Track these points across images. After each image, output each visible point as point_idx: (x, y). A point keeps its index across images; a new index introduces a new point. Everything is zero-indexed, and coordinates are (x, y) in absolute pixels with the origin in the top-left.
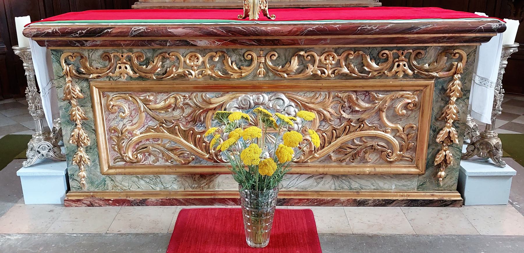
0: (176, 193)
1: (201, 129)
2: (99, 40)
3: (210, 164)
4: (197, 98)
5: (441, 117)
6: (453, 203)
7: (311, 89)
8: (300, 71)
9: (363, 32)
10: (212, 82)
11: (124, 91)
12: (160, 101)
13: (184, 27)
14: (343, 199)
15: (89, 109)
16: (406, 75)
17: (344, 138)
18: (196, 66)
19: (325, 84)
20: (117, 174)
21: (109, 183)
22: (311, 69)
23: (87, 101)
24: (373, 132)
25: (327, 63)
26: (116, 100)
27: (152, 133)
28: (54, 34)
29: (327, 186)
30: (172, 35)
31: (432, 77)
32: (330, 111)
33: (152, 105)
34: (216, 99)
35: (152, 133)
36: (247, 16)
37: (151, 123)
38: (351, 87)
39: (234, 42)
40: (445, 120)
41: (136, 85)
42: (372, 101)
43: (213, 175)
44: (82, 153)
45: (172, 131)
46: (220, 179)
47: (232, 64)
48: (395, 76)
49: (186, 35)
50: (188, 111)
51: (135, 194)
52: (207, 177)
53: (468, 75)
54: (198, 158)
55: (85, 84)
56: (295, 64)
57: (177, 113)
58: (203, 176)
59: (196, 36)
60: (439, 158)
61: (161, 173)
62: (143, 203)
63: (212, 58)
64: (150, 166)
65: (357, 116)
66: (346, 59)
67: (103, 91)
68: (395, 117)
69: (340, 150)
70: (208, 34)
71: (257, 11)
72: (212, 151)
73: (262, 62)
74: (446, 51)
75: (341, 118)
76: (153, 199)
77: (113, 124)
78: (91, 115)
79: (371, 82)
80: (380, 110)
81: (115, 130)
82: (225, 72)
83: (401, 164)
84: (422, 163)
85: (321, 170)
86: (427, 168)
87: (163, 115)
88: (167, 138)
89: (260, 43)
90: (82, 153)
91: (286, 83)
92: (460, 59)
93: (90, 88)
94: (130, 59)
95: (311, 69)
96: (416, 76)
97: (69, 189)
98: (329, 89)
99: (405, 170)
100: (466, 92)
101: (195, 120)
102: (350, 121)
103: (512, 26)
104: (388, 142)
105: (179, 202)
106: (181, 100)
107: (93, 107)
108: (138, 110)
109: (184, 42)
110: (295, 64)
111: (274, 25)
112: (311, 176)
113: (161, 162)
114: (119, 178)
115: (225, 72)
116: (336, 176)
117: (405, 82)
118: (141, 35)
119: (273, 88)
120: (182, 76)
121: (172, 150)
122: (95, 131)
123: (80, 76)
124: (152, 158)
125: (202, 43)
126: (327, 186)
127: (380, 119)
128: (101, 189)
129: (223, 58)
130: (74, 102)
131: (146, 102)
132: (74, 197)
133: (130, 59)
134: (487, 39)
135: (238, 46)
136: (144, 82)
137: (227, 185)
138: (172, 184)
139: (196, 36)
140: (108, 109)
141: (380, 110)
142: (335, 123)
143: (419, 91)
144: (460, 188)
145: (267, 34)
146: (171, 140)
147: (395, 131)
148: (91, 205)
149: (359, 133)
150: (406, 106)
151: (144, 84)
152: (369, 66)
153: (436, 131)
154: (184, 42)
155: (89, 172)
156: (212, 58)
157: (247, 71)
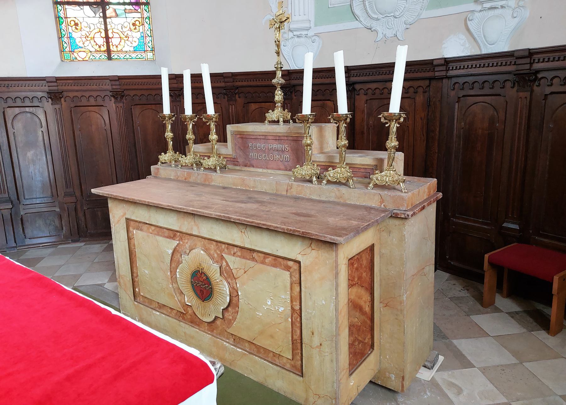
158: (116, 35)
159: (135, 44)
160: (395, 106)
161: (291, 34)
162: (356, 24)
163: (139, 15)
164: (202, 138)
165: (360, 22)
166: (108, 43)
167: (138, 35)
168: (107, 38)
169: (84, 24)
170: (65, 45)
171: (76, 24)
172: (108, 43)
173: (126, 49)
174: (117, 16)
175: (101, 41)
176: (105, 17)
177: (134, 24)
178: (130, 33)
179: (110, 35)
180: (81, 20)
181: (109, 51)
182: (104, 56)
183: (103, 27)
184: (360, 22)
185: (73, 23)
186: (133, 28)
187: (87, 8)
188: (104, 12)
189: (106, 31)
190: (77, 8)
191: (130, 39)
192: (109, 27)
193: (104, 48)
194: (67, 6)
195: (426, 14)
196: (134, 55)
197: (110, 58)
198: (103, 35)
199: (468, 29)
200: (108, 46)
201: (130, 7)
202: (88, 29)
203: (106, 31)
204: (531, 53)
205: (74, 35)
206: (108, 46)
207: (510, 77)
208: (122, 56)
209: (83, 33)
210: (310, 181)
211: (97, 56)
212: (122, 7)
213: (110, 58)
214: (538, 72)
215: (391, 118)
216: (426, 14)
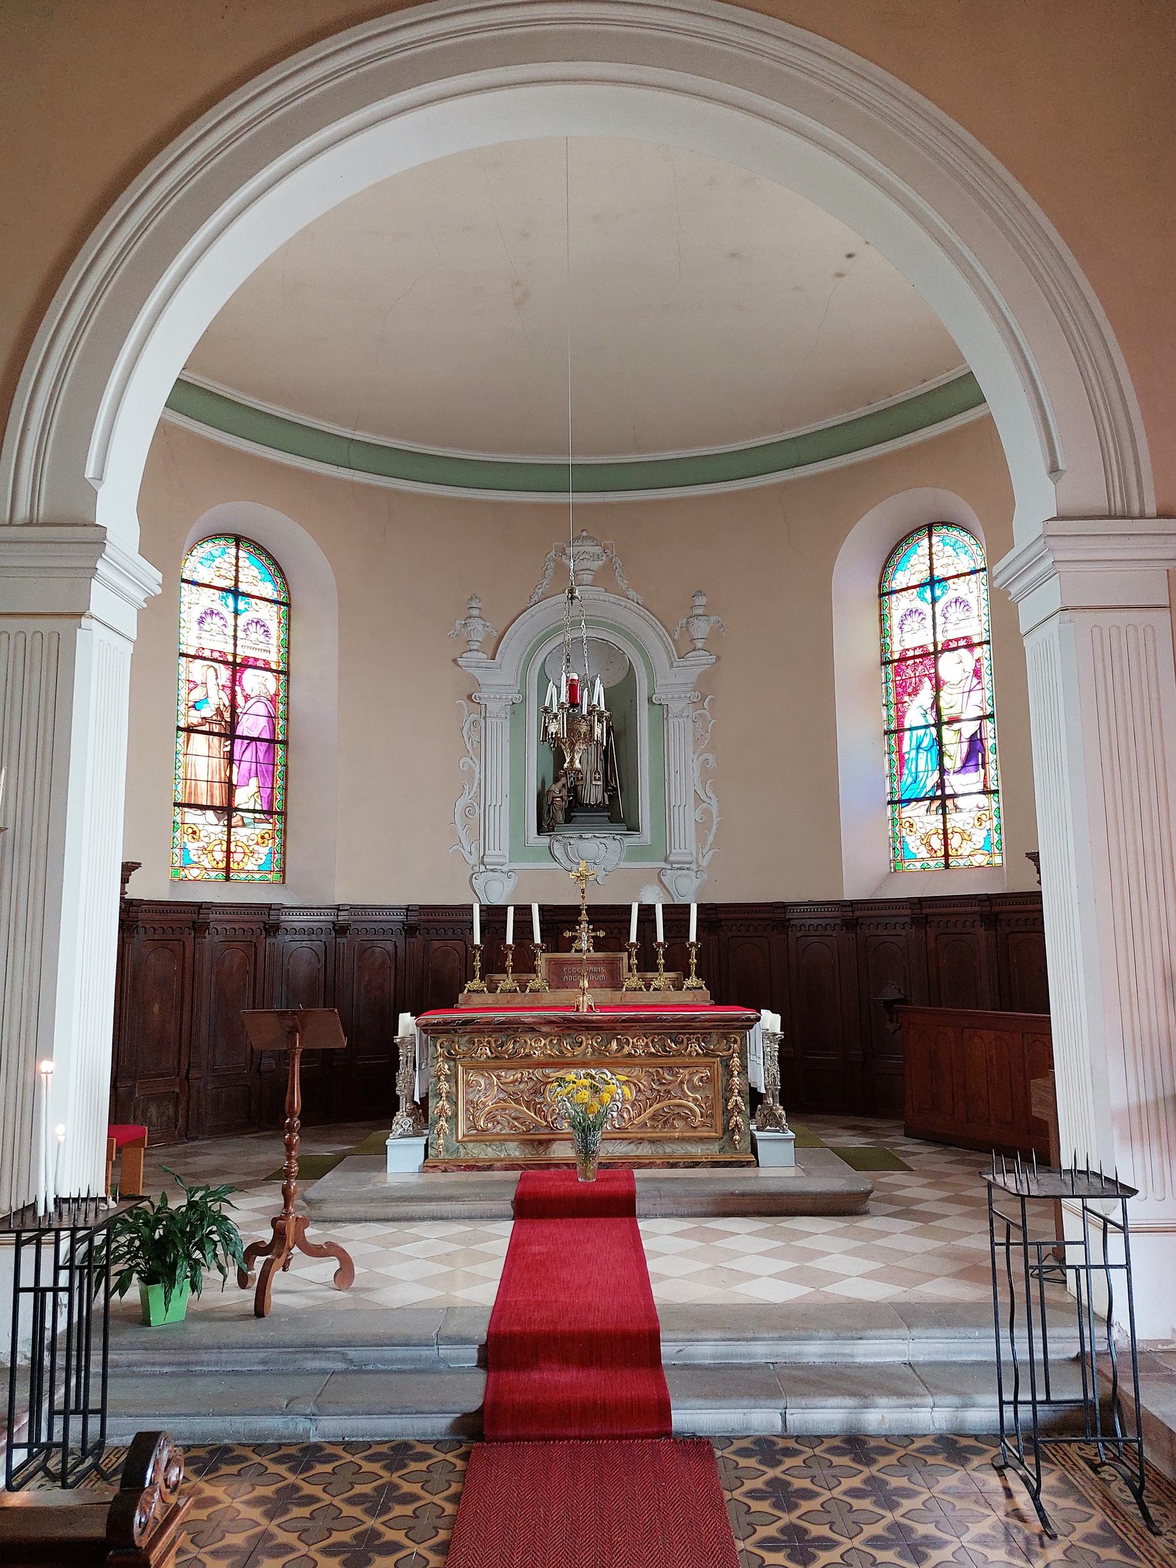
0: (518, 1159)
1: (541, 1100)
2: (469, 1028)
3: (546, 1131)
4: (538, 1073)
5: (728, 1090)
6: (748, 1164)
7: (628, 1065)
8: (618, 1051)
9: (661, 1020)
10: (551, 1060)
11: (479, 1068)
12: (510, 1076)
13: (533, 1017)
14: (658, 1161)
15: (453, 1084)
16: (698, 1054)
17: (656, 1106)
18: (539, 1047)
19: (637, 1061)
20: (469, 1141)
21: (462, 1150)
22: (626, 1049)
23: (452, 1078)
24: (677, 1101)
25: (638, 1045)
26: (472, 1077)
27: (503, 1104)
28: (438, 1024)
29: (645, 1150)
30: (525, 1023)
31: (718, 1056)
32: (644, 1083)
33: (504, 1080)
34: (554, 1074)
35: (503, 1104)
36: (578, 1010)
37: (501, 1096)
38: (661, 1062)
39: (568, 1028)
40: (732, 1091)
41: (492, 1064)
42: (675, 1075)
43: (550, 1141)
44: (443, 1122)
45: (517, 1101)
46: (555, 1146)
47: (115, 1275)
48: (690, 1055)
49: (534, 1023)
50: (531, 1084)
51: (484, 1160)
52: (545, 1143)
53: (743, 1055)
54: (537, 1126)
55: (452, 1064)
56: (614, 1045)
57: (521, 1086)
58: (540, 1142)
59: (540, 1024)
60: (732, 1124)
61: (506, 1140)
62: (490, 1168)
63: (551, 1041)
64: (498, 1134)
65: (665, 1087)
66: (652, 1041)
67: (466, 1072)
68: (694, 1088)
69: (653, 1117)
70: (550, 1022)
71: (586, 1006)
72: (549, 1119)
73: (589, 1043)
74: (725, 1036)
75: (652, 1089)
76: (498, 1164)
77: (471, 1097)
78: (454, 1089)
79: (672, 1060)
80: (682, 1082)
81: (472, 1102)
82: (561, 1052)
83: (704, 1128)
84: (720, 1131)
85: (639, 1135)
86: (724, 1133)
87: (511, 1089)
88: (513, 1108)
89: (588, 1028)
90: (443, 1122)
91: (608, 1060)
92: (735, 1042)
93: (456, 1066)
94: (489, 1042)
95: (626, 1049)
96: (705, 1055)
97: (426, 1156)
98: (642, 1066)
99: (706, 1134)
100: (744, 1068)
101: (536, 1092)
102: (659, 1091)
103: (771, 1021)
104: (691, 1110)
105: (519, 1167)
106: (526, 1073)
107: (457, 1082)
108: (491, 1084)
109: (531, 1029)
110: (614, 1045)
111: (598, 1015)
112: (631, 1141)
113: (507, 1131)
114: (470, 1145)
115: (561, 1052)
116: (652, 1141)
117: (697, 1060)
118: (502, 1023)
119: (599, 1065)
120: (528, 1056)
121: (516, 1119)
122: (456, 1104)
123: (450, 1058)
124: (499, 1127)
125: (545, 1029)
126: (645, 1150)
127: (683, 1090)
128: (454, 1156)
129: (559, 1041)
130: (442, 1078)
131: (499, 1077)
132: (429, 1164)
133: (489, 1042)
134: (751, 1027)
135: (571, 1032)
136: (499, 1061)
137: (563, 1151)
138: (514, 1151)
139: (540, 1024)
140: (468, 1084)
141: (682, 1082)
142: (648, 1093)
143: (709, 1066)
144: (754, 1151)
145: (592, 1022)
146: (516, 1110)
147: (695, 1100)
148: (445, 1171)
149: (667, 1102)
150: (701, 1079)
151: (499, 1063)
152: (670, 1047)
153: (727, 1100)
154: (531, 1029)
155: (446, 1140)
156: (551, 1041)
157: (578, 1051)
158: (239, 850)
159: (260, 862)
160: (693, 938)
161: (482, 868)
162: (555, 865)
163: (270, 826)
164: (525, 964)
165: (560, 863)
166: (228, 858)
167: (266, 850)
168: (228, 852)
169: (203, 833)
170: (176, 858)
171: (194, 833)
172: (228, 858)
173: (250, 867)
174: (244, 825)
175: (219, 856)
176: (229, 826)
177: (263, 837)
178: (256, 847)
179: (233, 849)
180: (201, 827)
181: (228, 869)
182: (222, 875)
183: (225, 838)
184: (560, 863)
185: (190, 831)
186: (260, 841)
187: (210, 813)
188: (229, 820)
189: (229, 842)
190: (199, 812)
191: (256, 855)
192: (232, 838)
193: (222, 865)
194: (186, 809)
195: (623, 865)
196: (257, 876)
197: (228, 879)
198: (224, 848)
199: (661, 881)
200: (228, 863)
201: (262, 816)
202: (207, 840)
203: (229, 842)
204: (783, 906)
205: (190, 846)
206: (228, 863)
207: (838, 921)
208: (243, 876)
209: (201, 844)
210: (641, 989)
211: (213, 874)
212: (251, 815)
213: (228, 879)
214: (721, 920)
215: (692, 945)
216: (623, 865)
